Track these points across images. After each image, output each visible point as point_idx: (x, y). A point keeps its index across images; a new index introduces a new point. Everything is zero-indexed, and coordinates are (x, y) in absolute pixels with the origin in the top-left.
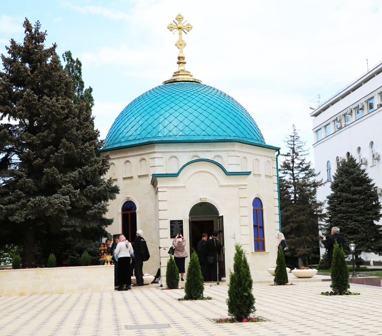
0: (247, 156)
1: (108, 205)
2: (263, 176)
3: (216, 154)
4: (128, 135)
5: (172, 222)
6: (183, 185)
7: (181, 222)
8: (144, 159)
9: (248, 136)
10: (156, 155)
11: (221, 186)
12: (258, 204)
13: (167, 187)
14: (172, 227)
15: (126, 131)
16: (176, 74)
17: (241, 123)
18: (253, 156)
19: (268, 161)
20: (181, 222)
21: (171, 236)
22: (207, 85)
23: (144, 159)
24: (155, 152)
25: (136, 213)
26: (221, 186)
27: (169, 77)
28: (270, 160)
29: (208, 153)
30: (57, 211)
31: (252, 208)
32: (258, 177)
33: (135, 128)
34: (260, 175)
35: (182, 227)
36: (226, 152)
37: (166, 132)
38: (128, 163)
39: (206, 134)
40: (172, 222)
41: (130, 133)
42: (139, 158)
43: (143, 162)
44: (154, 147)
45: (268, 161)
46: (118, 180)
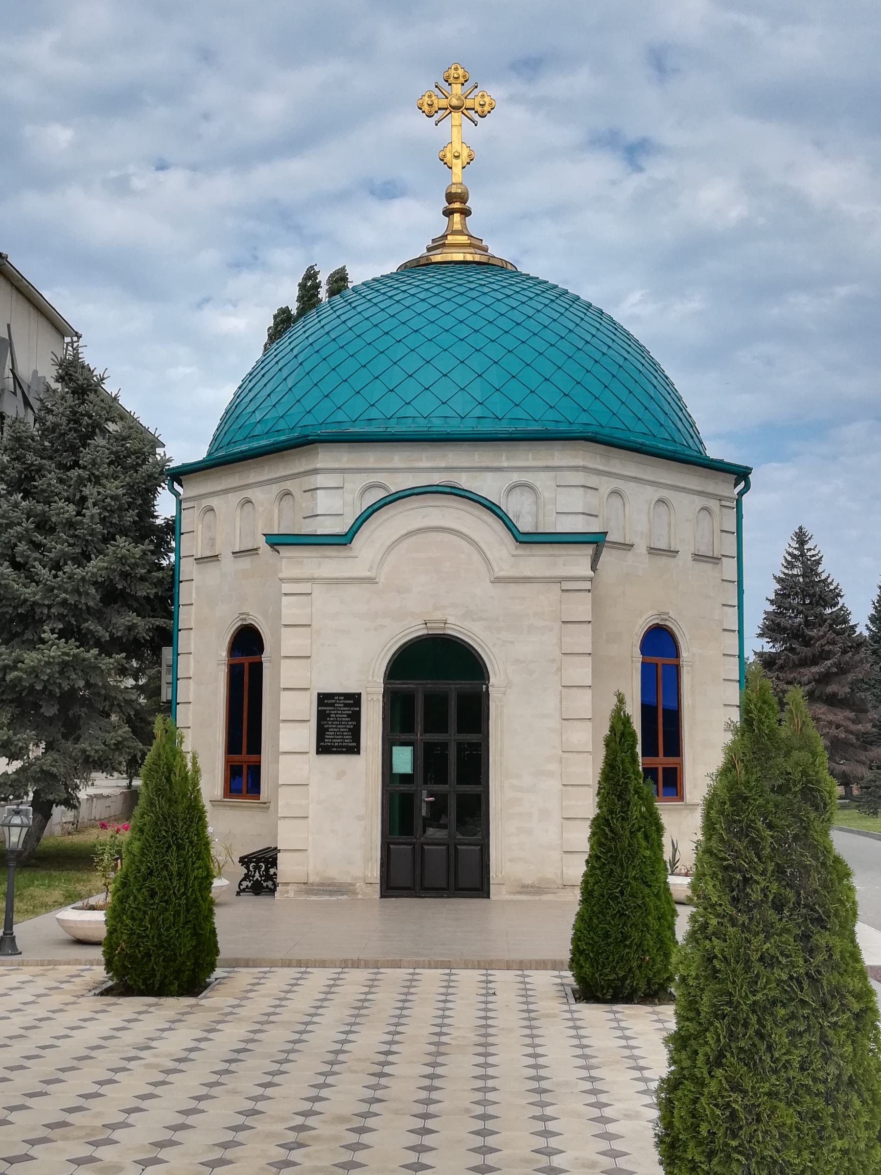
0: (628, 488)
1: (850, 613)
2: (685, 557)
3: (516, 477)
4: (253, 420)
5: (324, 699)
6: (368, 574)
7: (354, 700)
8: (288, 493)
9: (677, 436)
10: (320, 480)
11: (498, 580)
12: (867, 625)
13: (311, 580)
14: (322, 716)
15: (250, 409)
16: (439, 244)
17: (637, 390)
18: (649, 489)
19: (704, 509)
20: (354, 700)
21: (318, 746)
22: (552, 281)
23: (288, 493)
24: (316, 471)
25: (261, 663)
26: (498, 580)
27: (418, 251)
28: (714, 505)
29: (489, 475)
30: (37, 646)
31: (638, 657)
32: (663, 561)
33: (274, 399)
34: (698, 557)
35: (356, 717)
36: (551, 474)
37: (357, 407)
38: (249, 505)
39: (487, 413)
40: (324, 699)
41: (258, 416)
42: (275, 489)
43: (287, 502)
44: (320, 456)
45: (704, 509)
46: (221, 558)
